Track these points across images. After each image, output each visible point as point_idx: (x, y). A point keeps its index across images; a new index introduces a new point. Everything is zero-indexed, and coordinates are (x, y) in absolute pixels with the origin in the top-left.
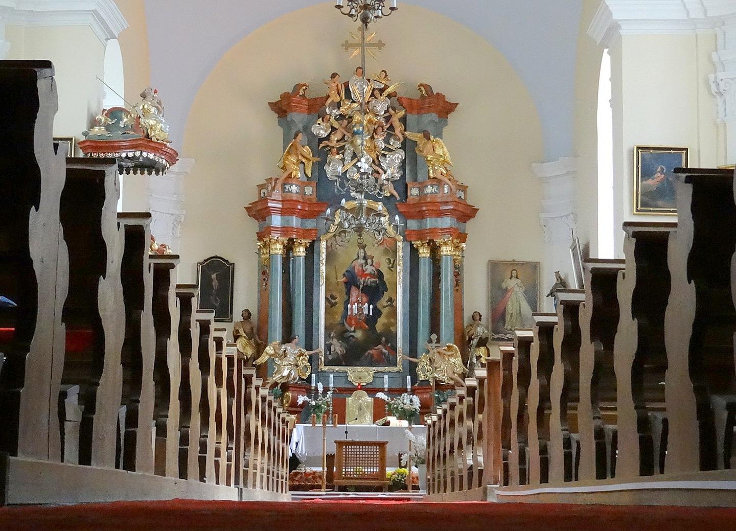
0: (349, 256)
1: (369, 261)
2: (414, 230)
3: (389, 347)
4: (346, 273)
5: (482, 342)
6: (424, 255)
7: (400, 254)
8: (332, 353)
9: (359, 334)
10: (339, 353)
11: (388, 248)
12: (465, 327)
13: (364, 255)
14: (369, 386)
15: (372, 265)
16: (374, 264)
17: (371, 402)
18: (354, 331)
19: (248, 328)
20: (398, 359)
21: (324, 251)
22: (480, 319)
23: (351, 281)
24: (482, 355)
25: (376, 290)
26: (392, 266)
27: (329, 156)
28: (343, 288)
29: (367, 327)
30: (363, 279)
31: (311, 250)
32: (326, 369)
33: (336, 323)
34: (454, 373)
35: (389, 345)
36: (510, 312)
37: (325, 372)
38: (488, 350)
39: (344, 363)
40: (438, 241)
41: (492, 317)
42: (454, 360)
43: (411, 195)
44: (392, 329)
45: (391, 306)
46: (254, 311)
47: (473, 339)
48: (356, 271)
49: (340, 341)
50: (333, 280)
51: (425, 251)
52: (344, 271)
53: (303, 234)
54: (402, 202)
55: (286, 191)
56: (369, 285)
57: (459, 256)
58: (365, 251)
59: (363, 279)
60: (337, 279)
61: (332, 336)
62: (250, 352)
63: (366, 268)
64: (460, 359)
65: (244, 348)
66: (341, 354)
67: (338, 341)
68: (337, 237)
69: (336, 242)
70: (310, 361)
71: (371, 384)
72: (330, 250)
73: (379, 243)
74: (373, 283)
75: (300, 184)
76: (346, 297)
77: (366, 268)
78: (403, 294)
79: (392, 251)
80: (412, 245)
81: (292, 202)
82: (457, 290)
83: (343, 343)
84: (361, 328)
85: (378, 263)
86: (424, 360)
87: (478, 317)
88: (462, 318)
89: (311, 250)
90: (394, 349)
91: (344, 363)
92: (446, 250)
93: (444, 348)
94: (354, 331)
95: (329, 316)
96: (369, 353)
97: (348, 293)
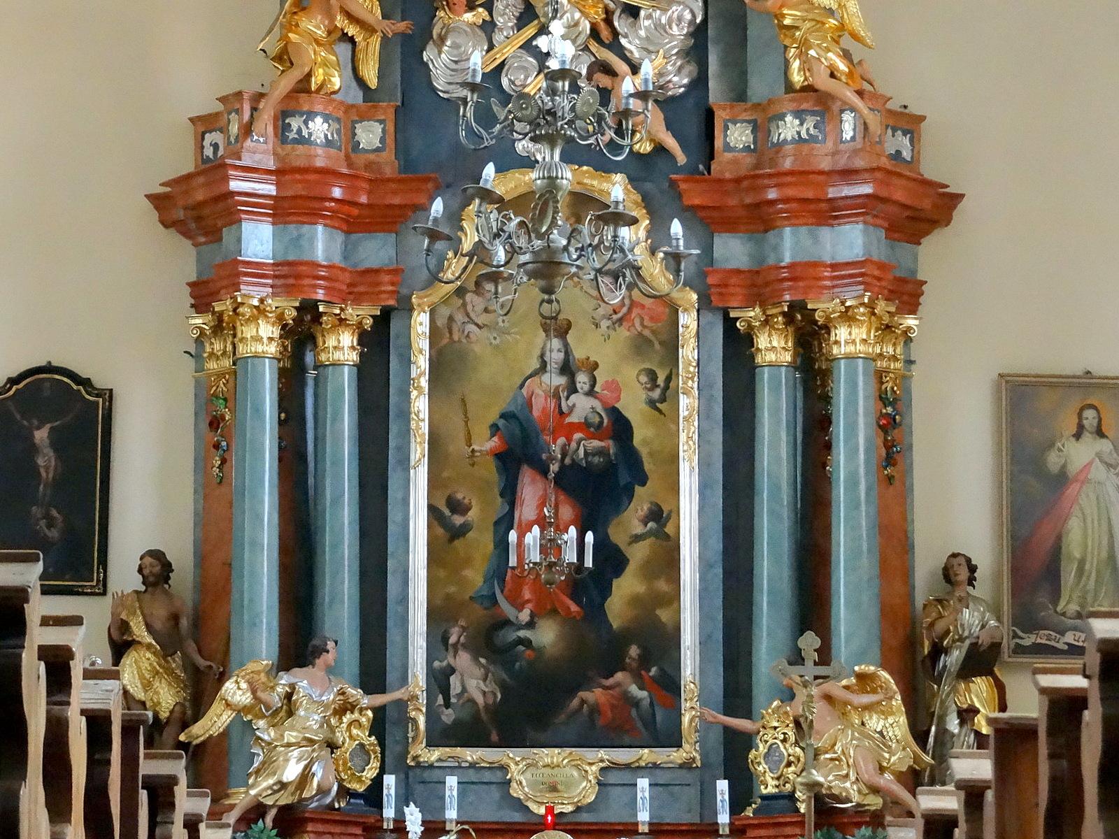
0: (511, 360)
1: (582, 379)
2: (738, 272)
4: (501, 423)
5: (981, 661)
6: (771, 357)
7: (688, 352)
8: (453, 700)
9: (547, 635)
10: (480, 700)
11: (647, 333)
13: (562, 355)
14: (585, 817)
15: (591, 393)
16: (597, 389)
18: (531, 625)
19: (160, 613)
20: (686, 720)
21: (424, 344)
22: (971, 581)
23: (519, 449)
24: (977, 705)
25: (606, 479)
26: (662, 397)
27: (440, 14)
28: (490, 472)
29: (574, 608)
30: (561, 440)
31: (378, 342)
33: (471, 593)
34: (882, 769)
35: (654, 671)
36: (1077, 555)
37: (431, 766)
38: (1000, 687)
39: (494, 737)
40: (823, 307)
41: (1015, 571)
42: (882, 723)
43: (728, 148)
44: (664, 615)
46: (181, 555)
47: (946, 651)
48: (536, 413)
49: (483, 661)
50: (457, 447)
51: (775, 344)
52: (493, 415)
53: (350, 285)
54: (697, 174)
55: (292, 135)
57: (894, 358)
58: (566, 345)
61: (453, 640)
62: (166, 698)
63: (570, 402)
64: (903, 719)
65: (147, 686)
66: (486, 706)
67: (475, 659)
68: (469, 297)
69: (468, 315)
70: (378, 727)
71: (590, 807)
72: (445, 341)
73: (615, 317)
74: (594, 455)
75: (340, 114)
77: (570, 402)
80: (729, 323)
81: (312, 177)
82: (890, 479)
83: (491, 668)
84: (554, 612)
85: (614, 387)
86: (776, 724)
87: (963, 574)
88: (907, 574)
89: (378, 342)
90: (670, 685)
91: (494, 737)
92: (849, 340)
93: (844, 682)
94: (531, 625)
95: (442, 573)
96: (583, 702)
97: (510, 493)
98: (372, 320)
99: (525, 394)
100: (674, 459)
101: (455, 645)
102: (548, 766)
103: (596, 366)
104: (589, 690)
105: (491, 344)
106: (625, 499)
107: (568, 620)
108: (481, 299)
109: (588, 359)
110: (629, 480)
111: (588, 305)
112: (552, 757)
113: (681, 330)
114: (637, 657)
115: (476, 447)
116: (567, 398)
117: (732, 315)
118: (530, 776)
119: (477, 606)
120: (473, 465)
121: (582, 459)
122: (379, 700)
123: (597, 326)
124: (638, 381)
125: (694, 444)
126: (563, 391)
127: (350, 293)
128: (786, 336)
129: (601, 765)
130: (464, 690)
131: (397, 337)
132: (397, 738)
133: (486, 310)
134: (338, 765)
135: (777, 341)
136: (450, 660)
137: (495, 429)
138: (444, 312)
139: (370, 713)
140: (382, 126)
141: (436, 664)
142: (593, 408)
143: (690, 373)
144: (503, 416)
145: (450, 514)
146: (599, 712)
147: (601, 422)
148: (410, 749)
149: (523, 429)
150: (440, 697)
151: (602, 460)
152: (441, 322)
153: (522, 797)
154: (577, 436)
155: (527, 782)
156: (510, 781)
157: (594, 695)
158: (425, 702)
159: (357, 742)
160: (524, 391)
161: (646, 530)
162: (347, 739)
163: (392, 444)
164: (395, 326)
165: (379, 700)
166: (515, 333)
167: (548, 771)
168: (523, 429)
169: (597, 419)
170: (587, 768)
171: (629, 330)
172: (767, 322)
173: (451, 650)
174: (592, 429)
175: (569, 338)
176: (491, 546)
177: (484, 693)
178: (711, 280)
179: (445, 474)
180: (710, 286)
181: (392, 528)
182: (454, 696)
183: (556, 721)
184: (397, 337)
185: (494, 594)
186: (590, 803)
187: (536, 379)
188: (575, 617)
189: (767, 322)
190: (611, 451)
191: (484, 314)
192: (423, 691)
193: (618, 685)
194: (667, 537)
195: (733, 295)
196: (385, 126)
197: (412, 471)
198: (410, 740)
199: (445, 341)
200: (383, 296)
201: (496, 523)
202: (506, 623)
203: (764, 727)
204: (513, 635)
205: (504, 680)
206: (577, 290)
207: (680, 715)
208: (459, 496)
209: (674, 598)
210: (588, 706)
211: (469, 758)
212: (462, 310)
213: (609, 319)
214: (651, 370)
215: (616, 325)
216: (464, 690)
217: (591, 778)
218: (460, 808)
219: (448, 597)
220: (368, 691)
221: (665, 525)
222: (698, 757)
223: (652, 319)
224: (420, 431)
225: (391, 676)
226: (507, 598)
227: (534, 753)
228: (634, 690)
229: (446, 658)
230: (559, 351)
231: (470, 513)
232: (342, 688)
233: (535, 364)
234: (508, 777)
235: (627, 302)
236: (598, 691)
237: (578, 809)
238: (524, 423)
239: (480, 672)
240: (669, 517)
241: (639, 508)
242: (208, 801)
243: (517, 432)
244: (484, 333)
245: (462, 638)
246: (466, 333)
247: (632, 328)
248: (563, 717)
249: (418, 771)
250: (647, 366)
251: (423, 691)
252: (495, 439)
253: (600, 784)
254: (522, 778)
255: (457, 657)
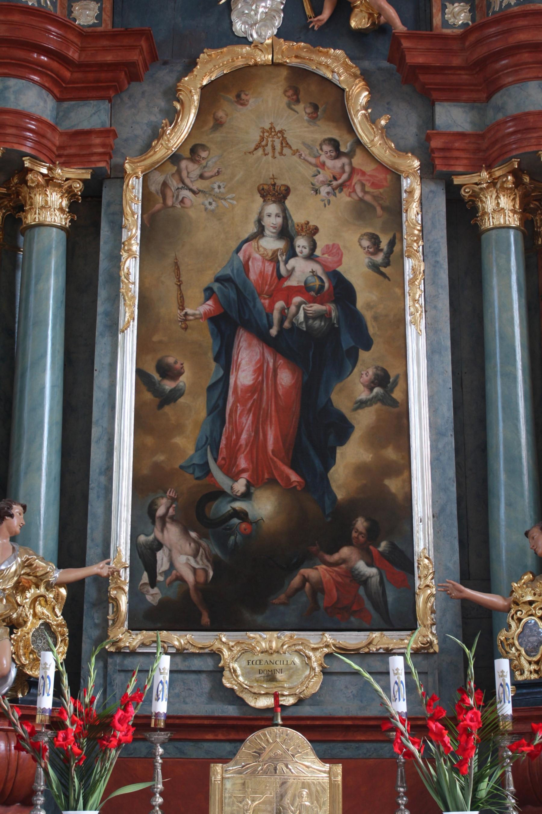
0: (228, 227)
1: (301, 243)
2: (462, 135)
3: (382, 554)
4: (216, 287)
7: (413, 213)
8: (160, 578)
9: (264, 507)
10: (189, 577)
11: (368, 198)
12: (141, 583)
13: (280, 220)
14: (307, 711)
15: (311, 257)
16: (318, 252)
17: (332, 784)
18: (247, 496)
20: (420, 601)
21: (137, 208)
23: (235, 312)
25: (332, 339)
26: (387, 262)
28: (204, 336)
29: (294, 477)
30: (280, 304)
31: (90, 210)
32: (133, 640)
35: (383, 545)
37: (133, 653)
39: (206, 619)
44: (393, 485)
45: (387, 400)
48: (253, 276)
49: (193, 534)
50: (169, 309)
52: (208, 279)
56: (304, 327)
58: (284, 210)
59: (280, 304)
60: (182, 307)
61: (161, 511)
63: (289, 266)
66: (196, 582)
67: (185, 532)
68: (184, 164)
69: (183, 182)
70: (73, 610)
71: (314, 699)
72: (159, 206)
73: (335, 183)
74: (315, 318)
76: (213, 371)
77: (289, 266)
78: (429, 358)
79: (383, 208)
81: (16, 18)
83: (203, 543)
84: (272, 482)
85: (335, 250)
86: (529, 598)
89: (90, 210)
90: (401, 561)
91: (206, 619)
94: (247, 496)
95: (149, 441)
96: (305, 580)
97: (225, 358)
98: (81, 184)
99: (242, 258)
100: (400, 324)
101: (163, 518)
102: (267, 651)
103: (316, 230)
104: (312, 566)
105: (206, 209)
106: (349, 364)
107: (289, 490)
108: (196, 166)
109: (308, 223)
110: (353, 344)
111: (308, 171)
112: (270, 641)
113: (404, 195)
114: (364, 531)
115: (189, 311)
116: (286, 262)
117: (457, 181)
118: (244, 663)
119: (188, 476)
120: (186, 329)
121: (301, 323)
122: (75, 574)
123: (317, 191)
124: (360, 245)
125: (421, 307)
126: (282, 254)
127: (59, 156)
128: (514, 199)
129: (326, 650)
130: (172, 566)
131: (109, 204)
132: (97, 621)
133: (201, 177)
134: (17, 648)
135: (505, 202)
136: (158, 533)
137: (209, 292)
138: (158, 178)
139: (63, 591)
140: (99, 5)
141: (142, 538)
142: (313, 272)
143: (415, 235)
144: (218, 280)
145: (160, 379)
146: (322, 591)
147: (322, 287)
148: (109, 634)
149: (239, 292)
150: (145, 575)
151: (323, 324)
152: (154, 188)
153: (236, 688)
154: (297, 299)
155: (241, 670)
156: (222, 669)
157: (316, 573)
158: (128, 581)
159: (41, 622)
160: (241, 255)
161: (371, 396)
162: (31, 618)
163: (100, 309)
164: (106, 195)
165: (75, 574)
166: (232, 199)
167: (265, 657)
168: (239, 292)
169: (318, 283)
170: (311, 654)
171: (350, 196)
172: (493, 184)
173: (158, 523)
174: (313, 293)
175: (288, 203)
176: (203, 414)
177: (194, 570)
178: (435, 143)
179: (155, 338)
180: (433, 151)
181: (98, 395)
182: (161, 574)
183: (276, 601)
184: (109, 204)
185: (207, 463)
186: (314, 694)
187: (253, 243)
188: (295, 487)
189: (493, 184)
190: (333, 314)
191: (200, 180)
192: (125, 568)
193: (344, 561)
194: (394, 403)
195: (457, 158)
196: (102, 4)
197: (120, 336)
198: (110, 622)
199: (159, 206)
200: (94, 158)
201: (210, 389)
202: (219, 494)
203: (516, 603)
204: (226, 507)
205: (216, 556)
206: (295, 158)
207: (414, 594)
208: (171, 360)
209: (405, 466)
210: (310, 584)
211: (176, 643)
212: (177, 177)
213: (329, 185)
214: (374, 234)
215: (337, 191)
216: (172, 566)
217: (315, 665)
218: (170, 704)
219: (157, 466)
220: (62, 563)
221: (392, 391)
222: (436, 642)
223: (373, 185)
224: (130, 294)
225: (92, 551)
226: (221, 467)
227: (249, 637)
228: (361, 566)
229: (153, 531)
230: (277, 215)
231: (182, 378)
232: (28, 559)
233: (252, 229)
234: (220, 665)
235: (347, 168)
236: (322, 568)
237: (300, 702)
238: (240, 287)
239: (189, 547)
240: (395, 383)
241: (364, 373)
242: (273, 700)
243: (233, 295)
244: (199, 199)
245: (171, 510)
246: (180, 198)
247: (353, 195)
248: (282, 597)
249: (118, 659)
250: (370, 230)
251: (125, 568)
252: (210, 302)
253: (325, 672)
254: (236, 666)
255: (165, 532)
